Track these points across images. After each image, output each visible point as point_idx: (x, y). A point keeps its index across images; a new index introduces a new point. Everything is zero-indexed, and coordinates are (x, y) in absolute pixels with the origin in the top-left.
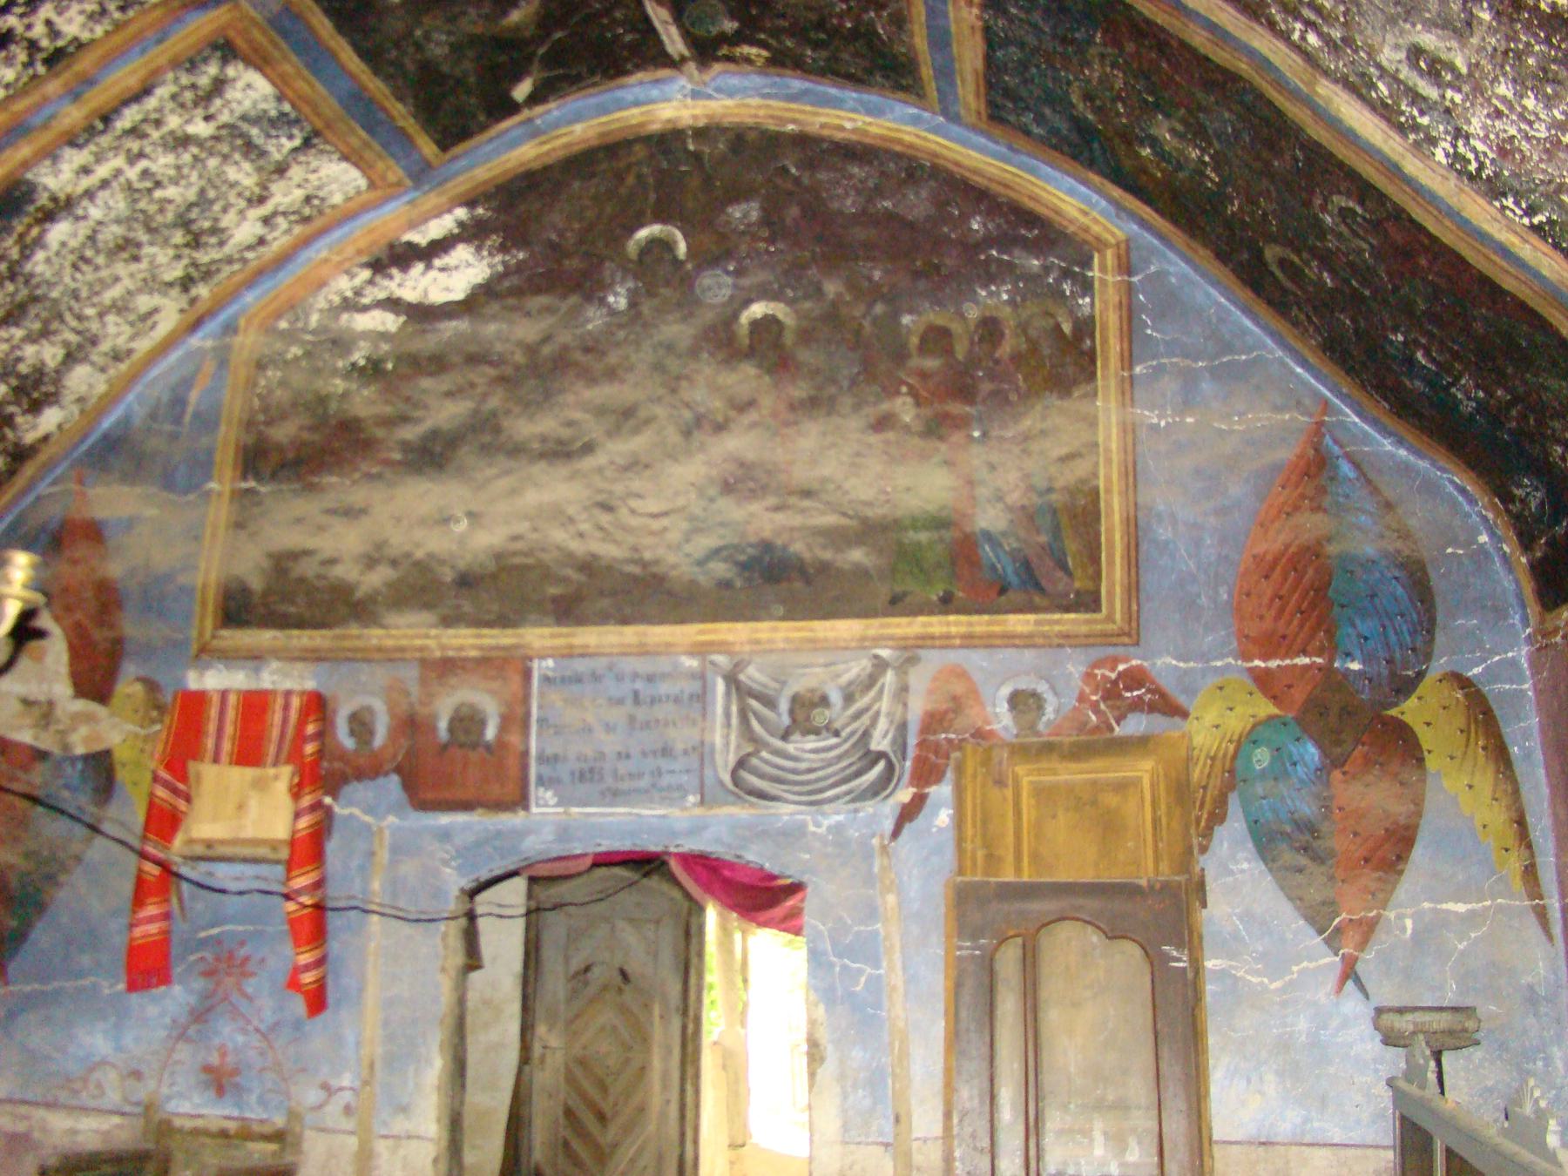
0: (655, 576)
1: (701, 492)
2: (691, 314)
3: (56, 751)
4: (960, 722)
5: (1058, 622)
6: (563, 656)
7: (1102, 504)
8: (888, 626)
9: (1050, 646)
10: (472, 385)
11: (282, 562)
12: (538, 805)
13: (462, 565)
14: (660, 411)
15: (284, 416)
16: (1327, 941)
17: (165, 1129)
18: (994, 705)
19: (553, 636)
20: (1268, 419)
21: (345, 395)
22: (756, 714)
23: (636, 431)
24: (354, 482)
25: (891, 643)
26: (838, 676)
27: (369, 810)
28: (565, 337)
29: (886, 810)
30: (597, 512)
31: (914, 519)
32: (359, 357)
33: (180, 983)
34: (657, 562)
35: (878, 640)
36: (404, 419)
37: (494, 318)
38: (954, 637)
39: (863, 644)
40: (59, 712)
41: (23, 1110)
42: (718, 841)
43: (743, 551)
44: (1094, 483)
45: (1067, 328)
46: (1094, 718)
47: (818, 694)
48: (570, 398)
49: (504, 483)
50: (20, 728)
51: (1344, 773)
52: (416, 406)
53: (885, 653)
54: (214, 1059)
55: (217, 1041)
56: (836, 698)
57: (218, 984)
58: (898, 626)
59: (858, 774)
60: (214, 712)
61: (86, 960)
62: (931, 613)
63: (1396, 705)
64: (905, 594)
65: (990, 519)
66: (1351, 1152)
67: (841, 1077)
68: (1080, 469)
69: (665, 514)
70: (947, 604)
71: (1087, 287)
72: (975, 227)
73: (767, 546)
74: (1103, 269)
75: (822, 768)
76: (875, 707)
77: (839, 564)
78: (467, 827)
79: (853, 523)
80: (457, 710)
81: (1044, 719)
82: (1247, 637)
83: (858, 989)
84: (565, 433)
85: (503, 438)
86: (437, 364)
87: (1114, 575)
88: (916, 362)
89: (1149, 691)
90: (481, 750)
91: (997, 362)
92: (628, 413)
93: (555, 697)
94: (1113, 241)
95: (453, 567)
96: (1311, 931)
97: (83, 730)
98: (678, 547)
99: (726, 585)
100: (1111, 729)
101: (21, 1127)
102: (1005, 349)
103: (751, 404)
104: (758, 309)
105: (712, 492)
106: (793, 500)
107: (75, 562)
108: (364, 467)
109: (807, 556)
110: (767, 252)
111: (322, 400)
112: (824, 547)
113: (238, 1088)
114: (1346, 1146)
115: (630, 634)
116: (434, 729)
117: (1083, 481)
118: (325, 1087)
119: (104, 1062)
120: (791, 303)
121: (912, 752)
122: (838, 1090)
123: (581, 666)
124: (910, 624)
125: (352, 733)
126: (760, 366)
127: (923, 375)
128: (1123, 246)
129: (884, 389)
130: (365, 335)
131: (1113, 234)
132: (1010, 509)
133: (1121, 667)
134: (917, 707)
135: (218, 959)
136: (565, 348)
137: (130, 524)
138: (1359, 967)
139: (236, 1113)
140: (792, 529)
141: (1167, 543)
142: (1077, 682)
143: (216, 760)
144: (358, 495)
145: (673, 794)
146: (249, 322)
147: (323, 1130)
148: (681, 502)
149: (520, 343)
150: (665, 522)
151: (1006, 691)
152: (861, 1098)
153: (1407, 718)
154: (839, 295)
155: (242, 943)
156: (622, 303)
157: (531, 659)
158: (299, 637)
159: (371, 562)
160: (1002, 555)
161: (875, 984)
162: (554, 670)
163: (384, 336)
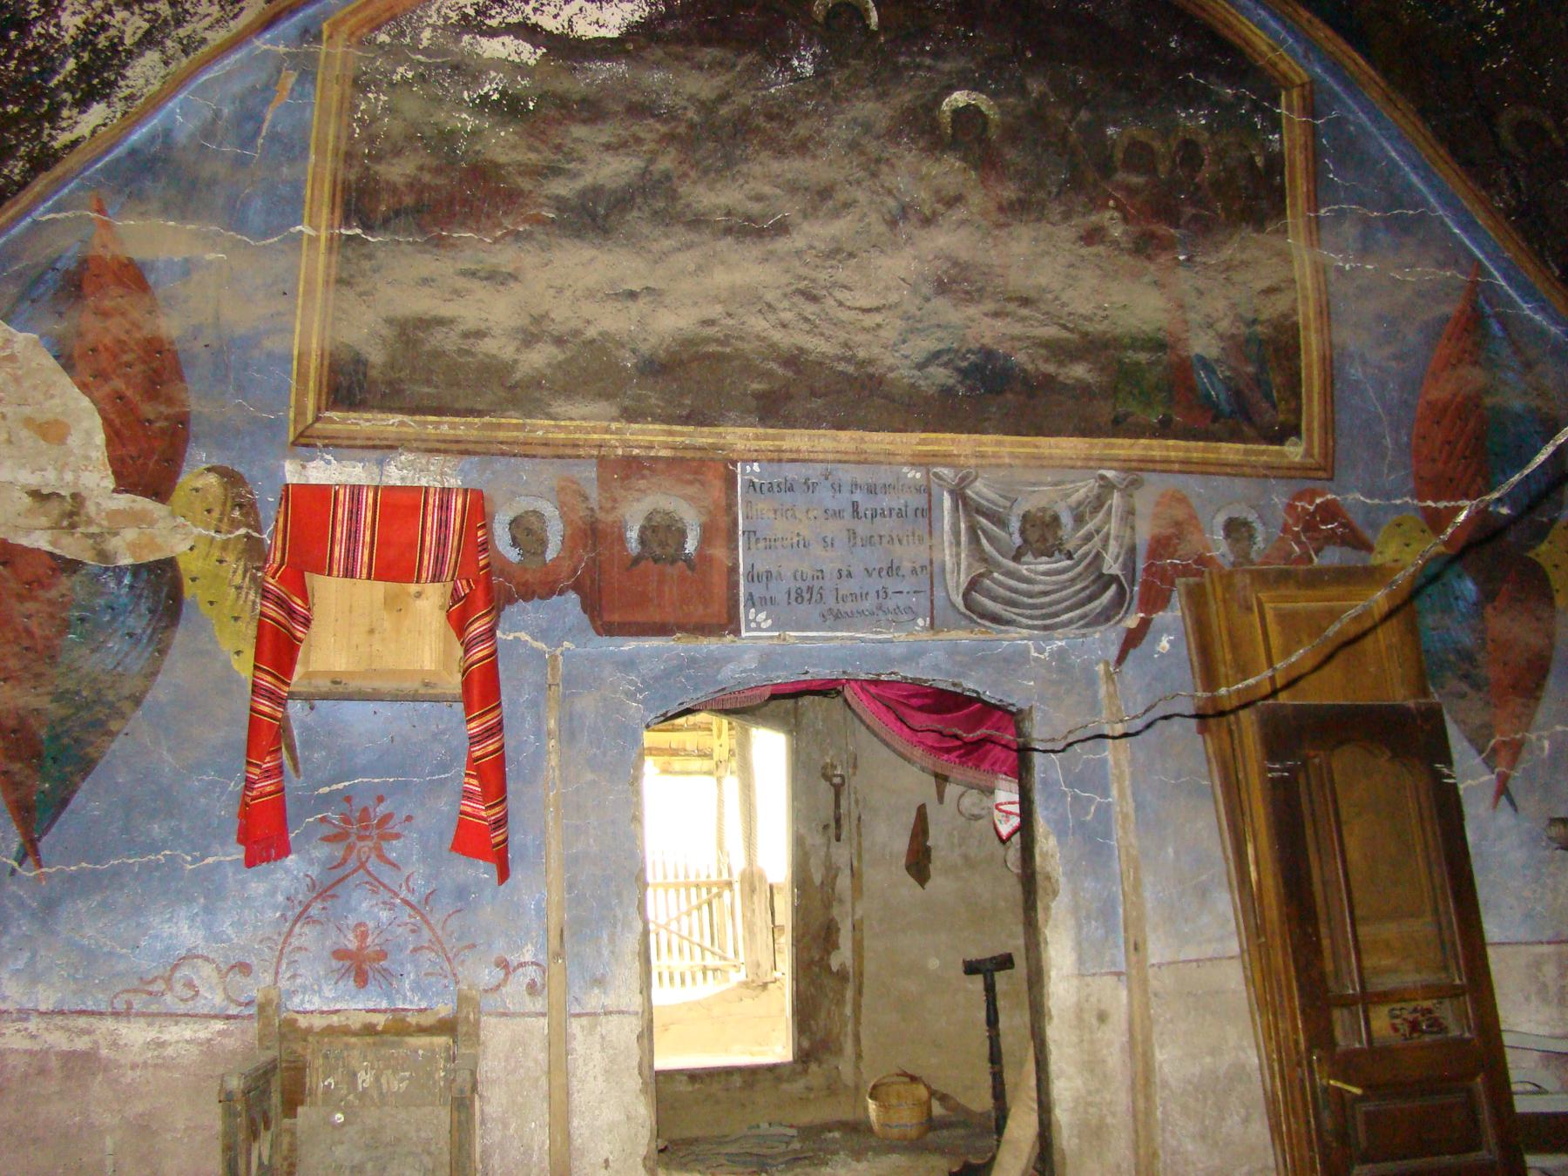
0: (871, 377)
1: (914, 289)
2: (885, 94)
3: (88, 558)
4: (1184, 548)
5: (1263, 453)
6: (771, 461)
7: (1302, 341)
8: (1112, 446)
9: (1258, 477)
10: (639, 141)
11: (410, 332)
12: (748, 629)
13: (645, 349)
14: (861, 196)
15: (397, 152)
16: (1486, 761)
17: (290, 1031)
18: (1212, 533)
19: (757, 437)
20: (1434, 273)
21: (476, 133)
22: (984, 532)
23: (836, 214)
24: (496, 241)
25: (1115, 464)
26: (1068, 496)
27: (542, 634)
28: (744, 99)
29: (1106, 640)
30: (799, 300)
31: (1134, 339)
32: (490, 87)
33: (298, 852)
34: (870, 362)
35: (1102, 461)
36: (555, 171)
37: (658, 65)
38: (1173, 462)
39: (1089, 464)
40: (91, 508)
41: (82, 1022)
42: (937, 668)
43: (964, 358)
44: (1295, 318)
45: (1259, 161)
46: (1296, 548)
47: (1050, 513)
48: (757, 169)
49: (687, 260)
50: (29, 531)
51: (1495, 608)
52: (569, 157)
53: (1110, 474)
54: (352, 943)
55: (352, 920)
56: (1066, 519)
57: (350, 848)
58: (1122, 447)
59: (1091, 598)
60: (342, 513)
61: (157, 830)
62: (1153, 436)
63: (1532, 547)
64: (1127, 415)
65: (1203, 345)
66: (1508, 949)
67: (1075, 909)
68: (1281, 304)
69: (878, 310)
70: (1164, 430)
71: (1275, 125)
72: (1173, 45)
73: (988, 354)
74: (1290, 108)
75: (1061, 590)
76: (1105, 530)
77: (1061, 378)
78: (656, 653)
79: (1075, 337)
80: (649, 518)
81: (1255, 547)
82: (1421, 478)
83: (1089, 818)
84: (756, 208)
85: (679, 206)
86: (591, 110)
87: (1313, 409)
88: (1120, 176)
89: (1341, 525)
90: (680, 563)
91: (1198, 187)
92: (825, 193)
93: (763, 505)
94: (1298, 81)
95: (634, 351)
96: (1473, 752)
97: (130, 534)
98: (894, 348)
99: (947, 391)
100: (1311, 560)
101: (82, 1044)
102: (1205, 174)
103: (958, 199)
104: (959, 98)
105: (926, 289)
106: (1011, 307)
107: (105, 314)
108: (508, 223)
109: (1030, 367)
110: (966, 37)
111: (449, 137)
112: (1047, 360)
113: (386, 974)
114: (1503, 944)
115: (847, 440)
116: (622, 539)
117: (1285, 316)
118: (503, 964)
119: (191, 956)
120: (993, 95)
121: (1140, 576)
122: (1073, 922)
123: (792, 472)
124: (1131, 446)
125: (515, 542)
126: (964, 159)
127: (1131, 191)
128: (1308, 87)
129: (1091, 200)
130: (498, 64)
131: (1298, 74)
132: (1221, 337)
133: (1318, 501)
134: (1144, 533)
135: (346, 820)
136: (747, 111)
137: (188, 268)
138: (1511, 785)
139: (384, 1005)
140: (1013, 338)
141: (1358, 382)
142: (1281, 516)
143: (349, 573)
144: (505, 257)
145: (900, 617)
146: (335, 27)
147: (504, 1014)
148: (893, 298)
149: (692, 98)
150: (878, 318)
151: (1221, 519)
152: (1095, 929)
153: (1540, 560)
154: (1043, 95)
155: (381, 799)
156: (809, 69)
157: (734, 463)
158: (437, 425)
159: (529, 339)
160: (1215, 381)
161: (1105, 811)
162: (760, 476)
163: (521, 68)
